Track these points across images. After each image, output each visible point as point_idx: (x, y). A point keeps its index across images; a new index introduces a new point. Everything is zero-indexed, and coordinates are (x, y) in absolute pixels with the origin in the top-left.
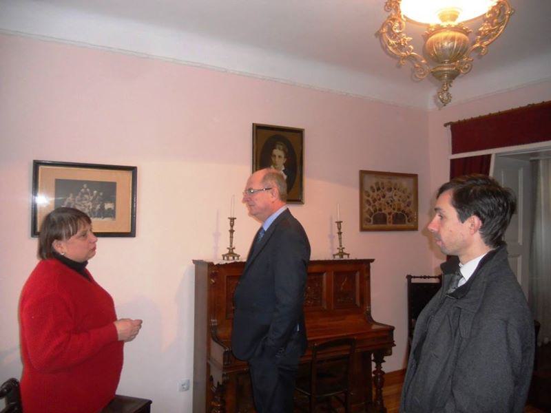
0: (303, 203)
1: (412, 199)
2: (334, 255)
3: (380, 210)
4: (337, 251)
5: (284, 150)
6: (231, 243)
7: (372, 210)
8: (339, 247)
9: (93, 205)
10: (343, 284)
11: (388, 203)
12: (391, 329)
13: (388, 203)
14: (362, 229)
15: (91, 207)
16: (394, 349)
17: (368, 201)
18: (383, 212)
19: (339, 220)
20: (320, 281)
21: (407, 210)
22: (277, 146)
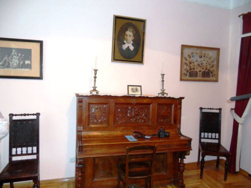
0: (143, 64)
1: (215, 63)
2: (159, 94)
3: (194, 69)
4: (161, 92)
5: (133, 32)
6: (163, 86)
7: (188, 69)
8: (162, 89)
9: (19, 61)
10: (163, 111)
11: (199, 65)
12: (190, 140)
13: (199, 65)
14: (181, 80)
15: (18, 63)
16: (191, 152)
17: (186, 63)
18: (196, 70)
19: (163, 73)
20: (149, 108)
21: (211, 70)
22: (129, 29)
